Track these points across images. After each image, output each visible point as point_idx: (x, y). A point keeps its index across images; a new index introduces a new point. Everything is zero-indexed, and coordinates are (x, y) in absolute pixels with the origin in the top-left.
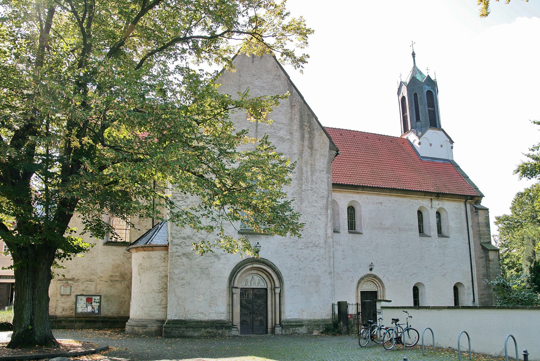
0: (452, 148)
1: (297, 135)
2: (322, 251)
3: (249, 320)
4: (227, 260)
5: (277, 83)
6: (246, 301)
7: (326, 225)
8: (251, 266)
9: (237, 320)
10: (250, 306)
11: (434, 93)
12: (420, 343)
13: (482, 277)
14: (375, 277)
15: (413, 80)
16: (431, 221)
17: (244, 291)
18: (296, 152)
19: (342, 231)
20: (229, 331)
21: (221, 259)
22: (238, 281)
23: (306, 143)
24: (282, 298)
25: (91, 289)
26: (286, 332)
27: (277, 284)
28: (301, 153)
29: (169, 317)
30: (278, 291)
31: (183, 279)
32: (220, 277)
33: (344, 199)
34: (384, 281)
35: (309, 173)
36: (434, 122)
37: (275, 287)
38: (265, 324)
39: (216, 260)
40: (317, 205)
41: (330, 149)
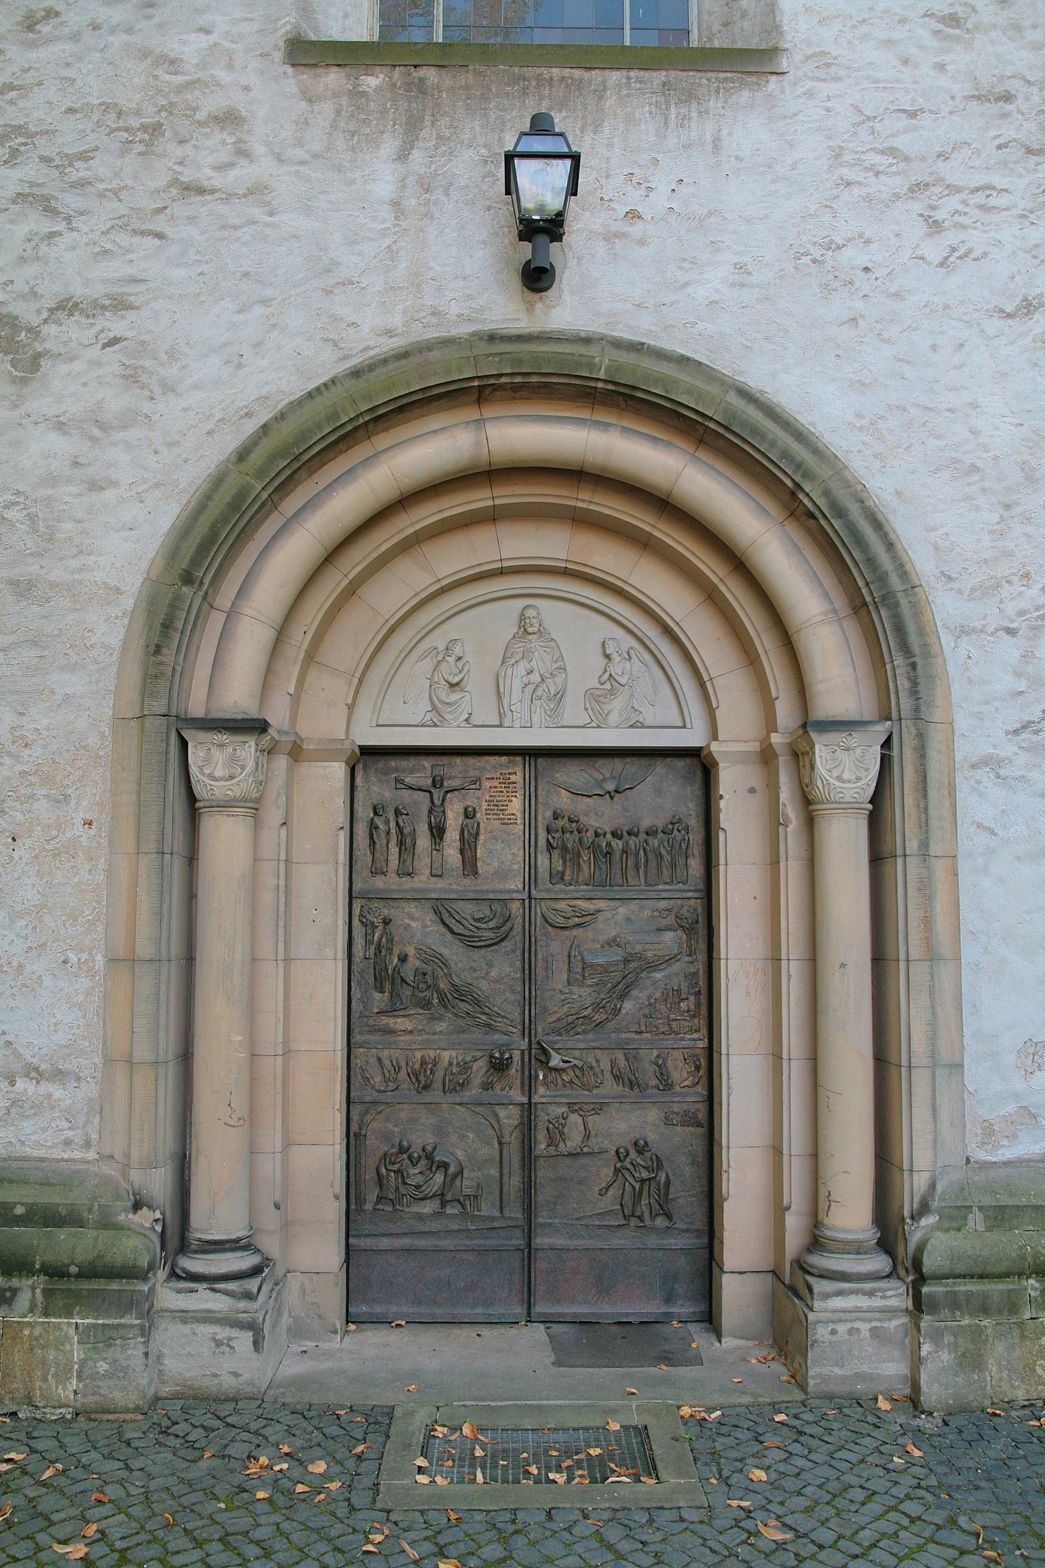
3: (471, 1141)
4: (132, 378)
6: (441, 910)
9: (281, 1155)
10: (495, 974)
17: (402, 786)
20: (99, 1339)
24: (906, 873)
26: (971, 1360)
27: (838, 673)
30: (845, 770)
38: (686, 1201)
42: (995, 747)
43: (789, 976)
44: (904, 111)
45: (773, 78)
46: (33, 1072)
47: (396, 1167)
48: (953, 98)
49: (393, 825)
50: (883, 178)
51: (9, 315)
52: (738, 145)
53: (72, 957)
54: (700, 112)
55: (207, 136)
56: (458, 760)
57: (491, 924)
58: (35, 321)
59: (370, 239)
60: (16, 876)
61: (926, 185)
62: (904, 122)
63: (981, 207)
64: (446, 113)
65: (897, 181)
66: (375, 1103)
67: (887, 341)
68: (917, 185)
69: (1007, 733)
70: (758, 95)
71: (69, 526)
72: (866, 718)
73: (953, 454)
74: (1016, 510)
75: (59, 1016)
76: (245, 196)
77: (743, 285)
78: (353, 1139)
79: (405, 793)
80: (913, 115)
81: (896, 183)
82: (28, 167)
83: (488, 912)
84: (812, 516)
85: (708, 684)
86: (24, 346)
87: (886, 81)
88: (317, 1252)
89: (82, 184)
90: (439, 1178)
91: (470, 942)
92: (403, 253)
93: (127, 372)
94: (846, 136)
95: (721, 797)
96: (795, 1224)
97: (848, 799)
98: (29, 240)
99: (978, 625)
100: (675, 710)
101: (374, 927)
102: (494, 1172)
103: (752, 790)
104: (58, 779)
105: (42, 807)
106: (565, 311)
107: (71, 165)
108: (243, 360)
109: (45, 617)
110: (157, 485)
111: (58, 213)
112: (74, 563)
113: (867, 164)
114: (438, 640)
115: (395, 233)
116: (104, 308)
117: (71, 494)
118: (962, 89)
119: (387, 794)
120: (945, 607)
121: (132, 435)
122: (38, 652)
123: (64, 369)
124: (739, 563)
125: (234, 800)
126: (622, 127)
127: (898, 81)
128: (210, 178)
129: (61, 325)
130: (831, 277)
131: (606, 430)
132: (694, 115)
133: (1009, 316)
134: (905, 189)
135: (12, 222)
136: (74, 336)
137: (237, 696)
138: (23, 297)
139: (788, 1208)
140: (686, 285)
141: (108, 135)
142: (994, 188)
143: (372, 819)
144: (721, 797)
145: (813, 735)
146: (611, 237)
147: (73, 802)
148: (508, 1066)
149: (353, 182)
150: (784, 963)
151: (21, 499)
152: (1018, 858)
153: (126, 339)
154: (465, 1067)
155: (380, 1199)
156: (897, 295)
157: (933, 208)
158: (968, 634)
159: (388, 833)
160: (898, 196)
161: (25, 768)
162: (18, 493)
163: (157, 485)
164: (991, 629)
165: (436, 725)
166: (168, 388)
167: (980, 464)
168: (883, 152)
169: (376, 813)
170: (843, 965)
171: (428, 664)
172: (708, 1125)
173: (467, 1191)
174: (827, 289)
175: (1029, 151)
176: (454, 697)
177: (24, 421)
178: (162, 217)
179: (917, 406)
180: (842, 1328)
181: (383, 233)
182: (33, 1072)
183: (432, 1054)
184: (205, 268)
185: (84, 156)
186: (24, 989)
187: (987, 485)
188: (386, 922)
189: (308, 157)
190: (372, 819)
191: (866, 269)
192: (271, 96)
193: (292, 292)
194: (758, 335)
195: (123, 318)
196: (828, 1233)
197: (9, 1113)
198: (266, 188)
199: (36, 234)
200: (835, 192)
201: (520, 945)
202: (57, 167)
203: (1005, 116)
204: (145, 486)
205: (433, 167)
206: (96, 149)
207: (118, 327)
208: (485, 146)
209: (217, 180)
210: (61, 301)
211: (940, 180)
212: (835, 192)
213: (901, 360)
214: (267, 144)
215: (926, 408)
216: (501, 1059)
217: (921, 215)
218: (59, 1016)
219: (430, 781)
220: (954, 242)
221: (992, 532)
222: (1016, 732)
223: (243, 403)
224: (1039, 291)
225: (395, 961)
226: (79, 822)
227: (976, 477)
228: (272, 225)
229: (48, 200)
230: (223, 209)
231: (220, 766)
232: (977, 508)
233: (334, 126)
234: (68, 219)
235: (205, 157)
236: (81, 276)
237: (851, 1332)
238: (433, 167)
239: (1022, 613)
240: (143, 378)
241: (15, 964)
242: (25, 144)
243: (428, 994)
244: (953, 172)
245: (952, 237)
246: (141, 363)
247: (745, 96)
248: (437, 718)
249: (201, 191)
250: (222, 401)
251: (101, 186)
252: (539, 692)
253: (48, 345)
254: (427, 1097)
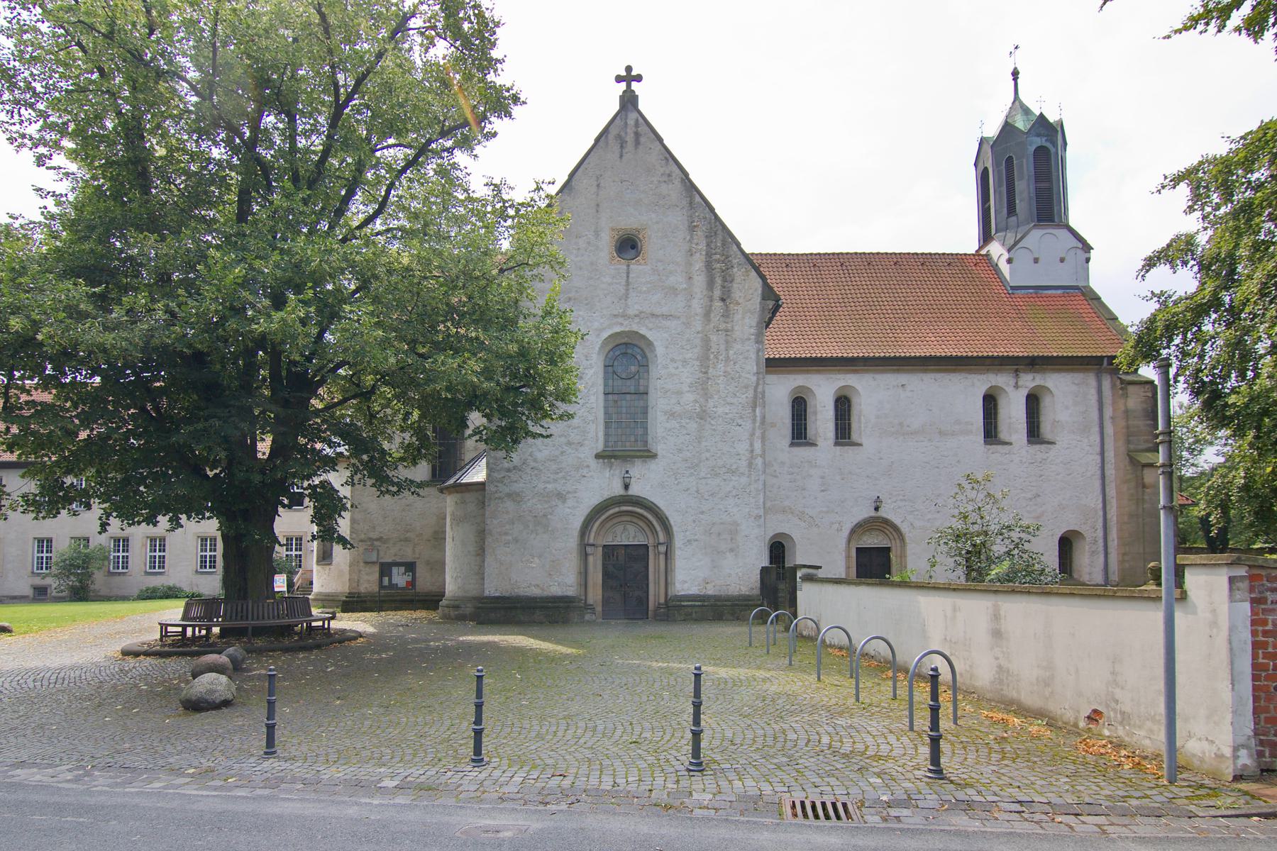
0: (1088, 260)
1: (700, 280)
2: (744, 480)
5: (664, 189)
7: (753, 434)
8: (617, 510)
9: (595, 595)
11: (1053, 150)
13: (1126, 518)
14: (886, 522)
15: (1008, 128)
16: (1013, 411)
17: (609, 551)
18: (699, 311)
19: (820, 442)
22: (597, 534)
23: (717, 293)
25: (408, 555)
27: (662, 537)
28: (707, 315)
29: (487, 593)
30: (662, 549)
31: (506, 534)
33: (781, 389)
34: (904, 528)
35: (722, 347)
36: (1049, 208)
39: (559, 503)
40: (735, 401)
41: (764, 298)
88: (599, 609)
106: (630, 492)
120: (675, 529)
137: (591, 541)
172: (647, 592)
192: (593, 463)
235: (585, 472)
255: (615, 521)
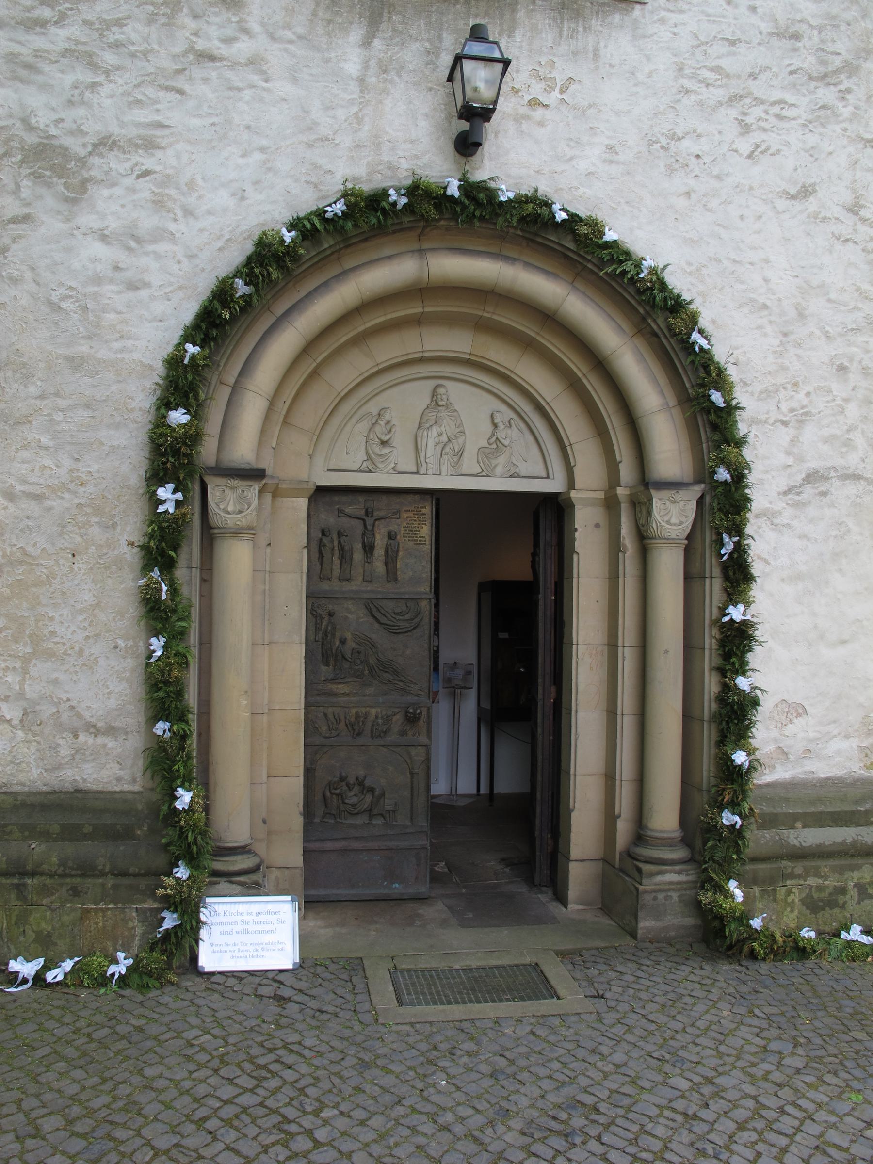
4: (159, 203)
6: (372, 607)
12: (646, 868)
17: (345, 517)
21: (100, 194)
22: (281, 412)
27: (669, 448)
32: (76, 364)
37: (646, 483)
39: (46, 203)
42: (771, 503)
43: (624, 657)
44: (727, 40)
45: (638, 7)
46: (93, 729)
47: (337, 791)
48: (761, 33)
49: (336, 543)
50: (711, 89)
51: (61, 147)
52: (611, 55)
53: (121, 643)
54: (585, 28)
55: (216, 14)
56: (384, 497)
57: (407, 617)
58: (82, 152)
59: (342, 107)
60: (76, 582)
61: (741, 96)
62: (725, 49)
63: (778, 117)
64: (400, 13)
65: (721, 91)
66: (323, 746)
67: (710, 210)
68: (735, 96)
69: (779, 494)
70: (626, 18)
71: (112, 316)
72: (686, 480)
73: (752, 296)
74: (791, 338)
75: (111, 688)
76: (246, 65)
77: (611, 162)
78: (309, 772)
79: (345, 520)
80: (733, 43)
81: (718, 94)
82: (73, 28)
83: (404, 608)
84: (656, 335)
85: (568, 448)
86: (74, 173)
87: (715, 16)
89: (117, 45)
90: (368, 798)
91: (391, 630)
92: (366, 119)
93: (156, 198)
94: (687, 55)
95: (576, 530)
96: (623, 828)
97: (673, 536)
98: (76, 88)
99: (763, 417)
100: (541, 465)
101: (322, 618)
102: (407, 794)
103: (597, 526)
104: (107, 510)
105: (95, 532)
107: (108, 29)
108: (245, 194)
109: (94, 386)
110: (180, 288)
111: (100, 67)
112: (117, 345)
113: (700, 77)
114: (373, 408)
115: (361, 103)
116: (137, 146)
117: (112, 292)
118: (766, 27)
119: (332, 520)
121: (163, 247)
122: (91, 413)
123: (106, 192)
124: (601, 365)
125: (242, 528)
126: (529, 34)
127: (724, 17)
128: (219, 48)
129: (103, 157)
130: (673, 160)
131: (513, 264)
132: (581, 29)
133: (793, 197)
134: (726, 98)
135: (62, 72)
136: (113, 166)
137: (243, 449)
138: (71, 133)
139: (619, 816)
140: (571, 159)
141: (138, 7)
142: (786, 103)
143: (321, 540)
144: (576, 530)
145: (653, 492)
146: (519, 119)
147: (119, 528)
148: (419, 719)
149: (328, 60)
150: (620, 649)
151: (74, 293)
152: (783, 580)
153: (155, 172)
154: (388, 719)
155: (325, 815)
156: (718, 177)
157: (745, 114)
158: (757, 424)
159: (333, 549)
160: (720, 104)
161: (82, 501)
162: (71, 288)
163: (180, 288)
164: (771, 421)
165: (370, 471)
166: (188, 212)
167: (768, 303)
168: (712, 70)
169: (323, 534)
170: (666, 652)
171: (364, 426)
173: (388, 808)
174: (671, 170)
175: (811, 78)
176: (386, 451)
177: (75, 232)
178: (181, 77)
179: (729, 259)
180: (661, 896)
181: (352, 102)
182: (93, 729)
183: (364, 710)
184: (215, 120)
185: (119, 23)
186: (85, 668)
187: (772, 318)
188: (331, 614)
189: (294, 38)
190: (321, 540)
191: (698, 156)
193: (283, 144)
194: (622, 200)
195: (153, 155)
196: (649, 833)
197: (73, 759)
198: (262, 59)
199: (82, 83)
200: (677, 97)
201: (427, 632)
202: (97, 30)
203: (795, 50)
204: (171, 288)
205: (389, 53)
206: (129, 18)
207: (148, 163)
208: (428, 40)
209: (224, 51)
210: (103, 138)
211: (749, 94)
212: (677, 97)
213: (719, 225)
214: (263, 24)
215: (735, 261)
216: (414, 713)
217: (737, 119)
218: (111, 688)
219: (363, 512)
220: (758, 141)
221: (775, 352)
222: (785, 493)
223: (246, 228)
224: (813, 181)
225: (337, 643)
226: (123, 542)
227: (766, 313)
228: (267, 90)
229: (90, 56)
230: (229, 74)
231: (231, 503)
232: (765, 335)
233: (314, 14)
234: (107, 73)
236: (118, 119)
237: (666, 898)
238: (389, 53)
239: (792, 410)
240: (170, 204)
241: (77, 649)
242: (71, 9)
243: (361, 667)
244: (758, 88)
245: (756, 137)
246: (167, 191)
247: (617, 17)
248: (371, 466)
249: (212, 58)
250: (230, 225)
251: (133, 48)
252: (447, 449)
253: (92, 173)
254: (360, 741)
255: (389, 349)
